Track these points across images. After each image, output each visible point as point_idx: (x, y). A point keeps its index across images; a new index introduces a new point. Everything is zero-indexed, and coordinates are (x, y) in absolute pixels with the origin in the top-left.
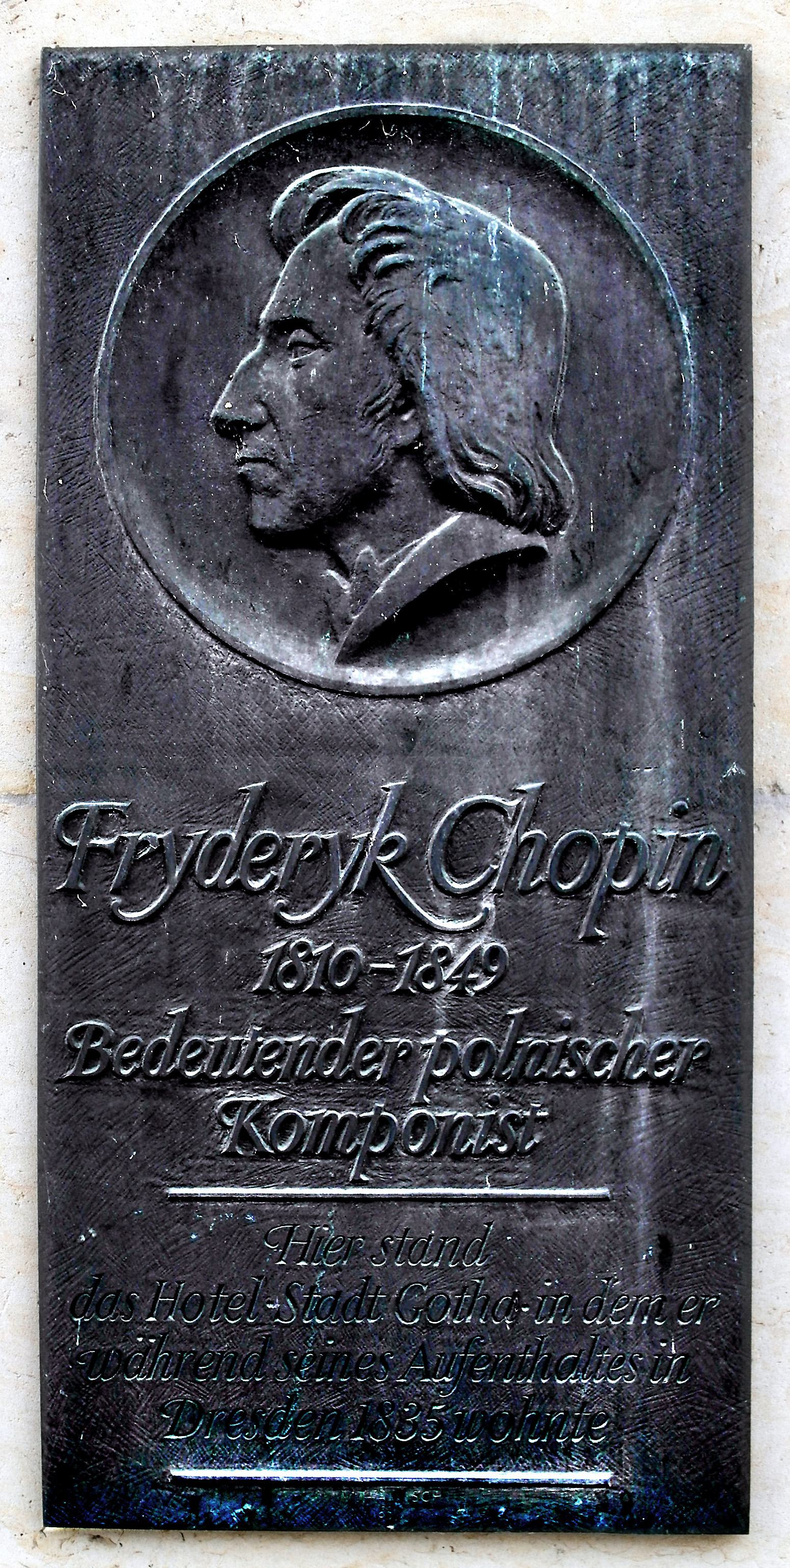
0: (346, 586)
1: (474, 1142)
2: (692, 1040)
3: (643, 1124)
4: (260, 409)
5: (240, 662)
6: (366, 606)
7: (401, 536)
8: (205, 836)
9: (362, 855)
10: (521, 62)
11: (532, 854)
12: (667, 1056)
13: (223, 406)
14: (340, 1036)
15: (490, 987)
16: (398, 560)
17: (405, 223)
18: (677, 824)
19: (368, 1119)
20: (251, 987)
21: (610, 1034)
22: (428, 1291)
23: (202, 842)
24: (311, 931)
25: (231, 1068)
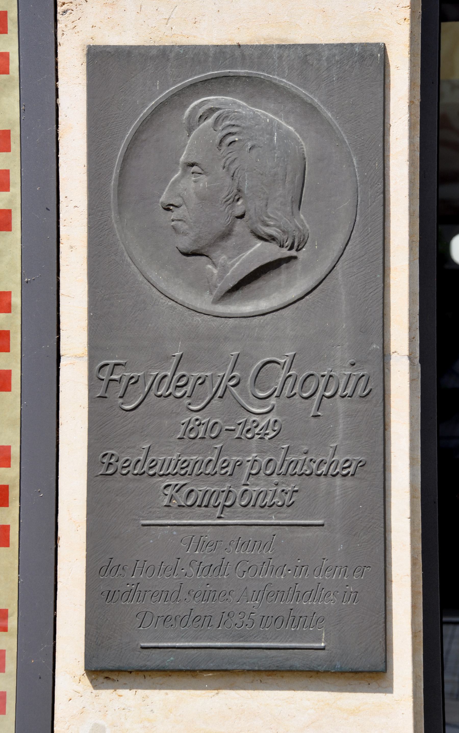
0: (215, 271)
1: (268, 501)
3: (338, 493)
4: (180, 199)
5: (172, 303)
6: (223, 280)
7: (238, 251)
8: (157, 375)
10: (287, 52)
11: (291, 380)
13: (164, 198)
14: (213, 456)
16: (237, 261)
17: (238, 123)
18: (350, 369)
20: (176, 436)
21: (324, 456)
22: (249, 564)
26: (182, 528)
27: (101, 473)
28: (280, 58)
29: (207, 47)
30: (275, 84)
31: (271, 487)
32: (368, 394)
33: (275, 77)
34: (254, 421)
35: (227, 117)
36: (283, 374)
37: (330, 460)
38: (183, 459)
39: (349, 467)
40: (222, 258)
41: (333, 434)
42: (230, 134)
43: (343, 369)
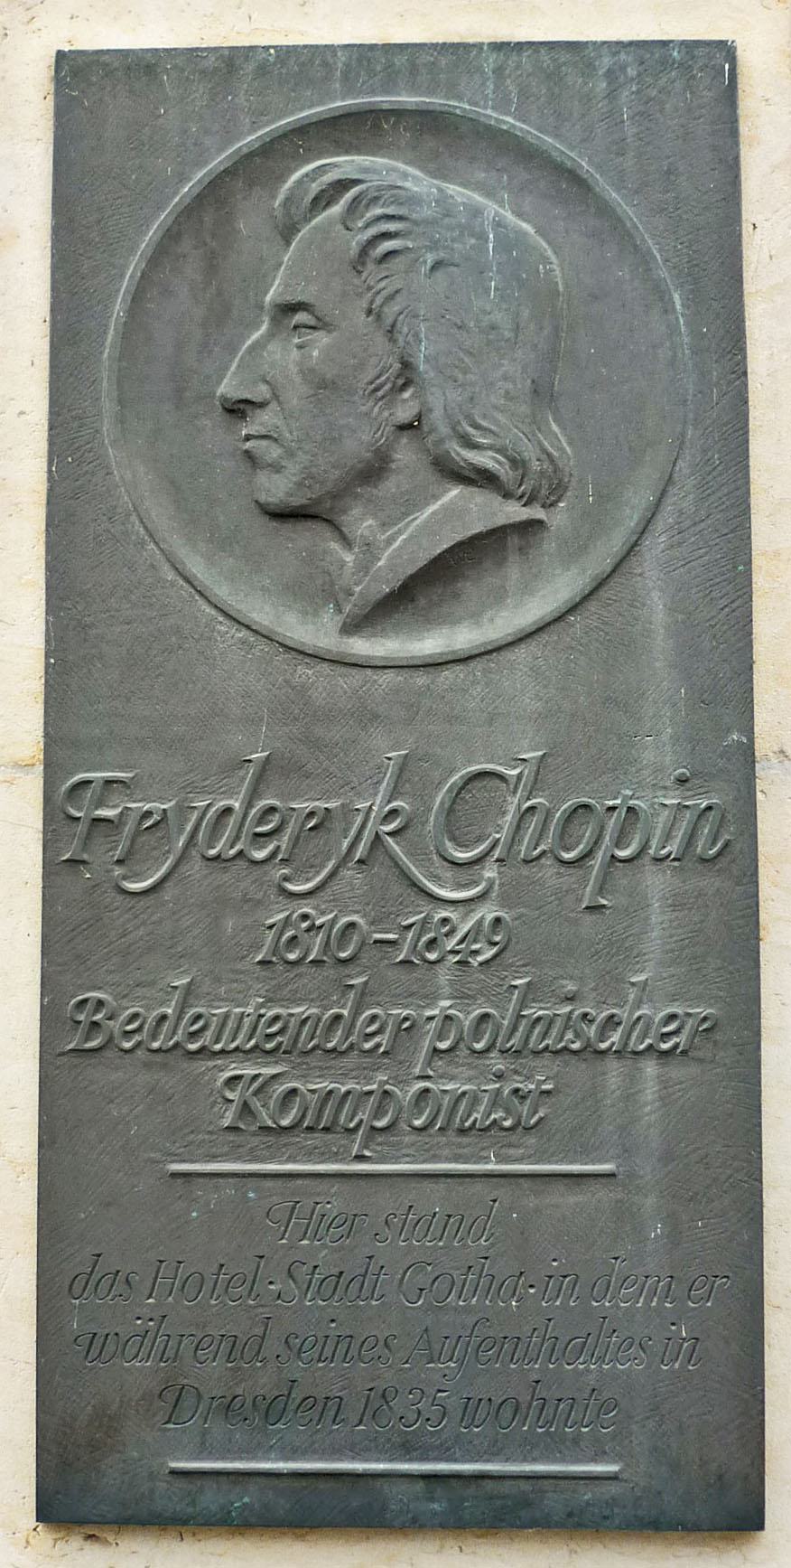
0: (349, 558)
5: (243, 633)
11: (533, 823)
13: (228, 387)
16: (400, 532)
21: (616, 1005)
26: (269, 1184)
27: (71, 1046)
28: (499, 71)
29: (331, 49)
30: (488, 128)
31: (487, 1083)
32: (719, 854)
33: (489, 112)
34: (445, 921)
35: (376, 199)
36: (513, 804)
37: (631, 1013)
38: (271, 1013)
39: (676, 1032)
40: (362, 523)
41: (635, 952)
42: (386, 236)
43: (659, 793)
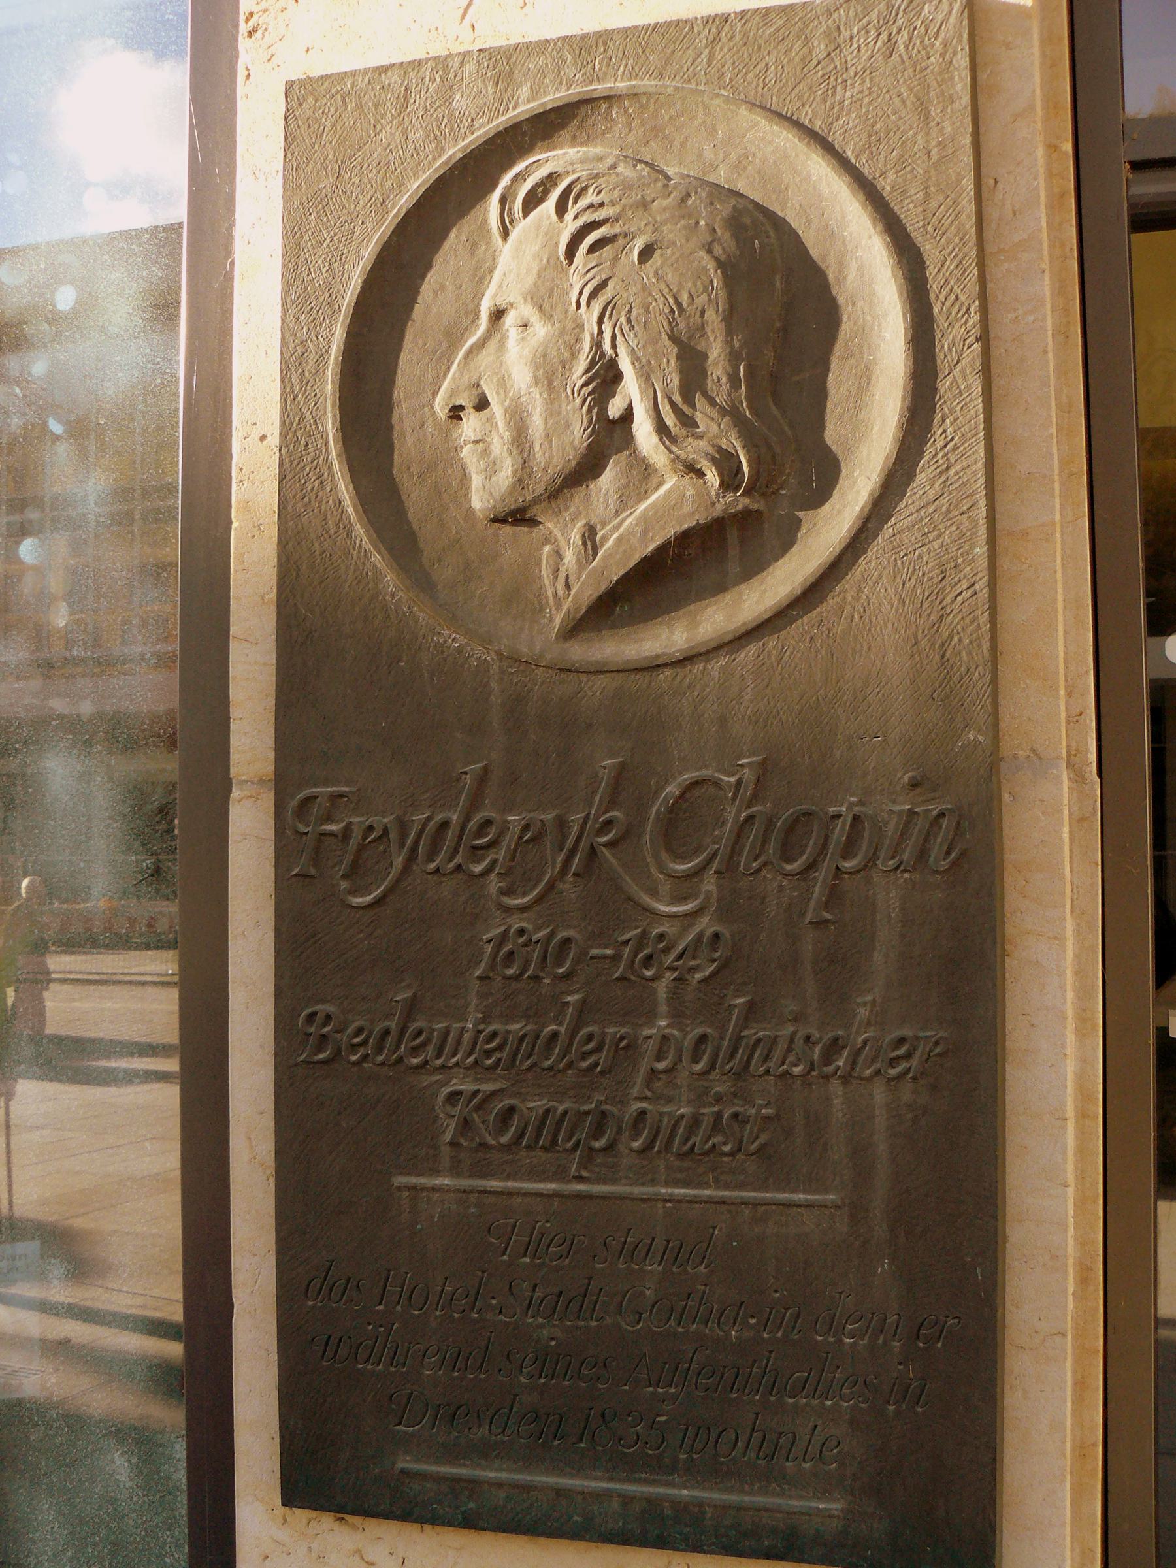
2: (929, 1034)
8: (429, 819)
9: (579, 838)
12: (902, 1051)
15: (713, 975)
19: (587, 1113)
23: (425, 825)
24: (531, 915)
25: (454, 1055)
